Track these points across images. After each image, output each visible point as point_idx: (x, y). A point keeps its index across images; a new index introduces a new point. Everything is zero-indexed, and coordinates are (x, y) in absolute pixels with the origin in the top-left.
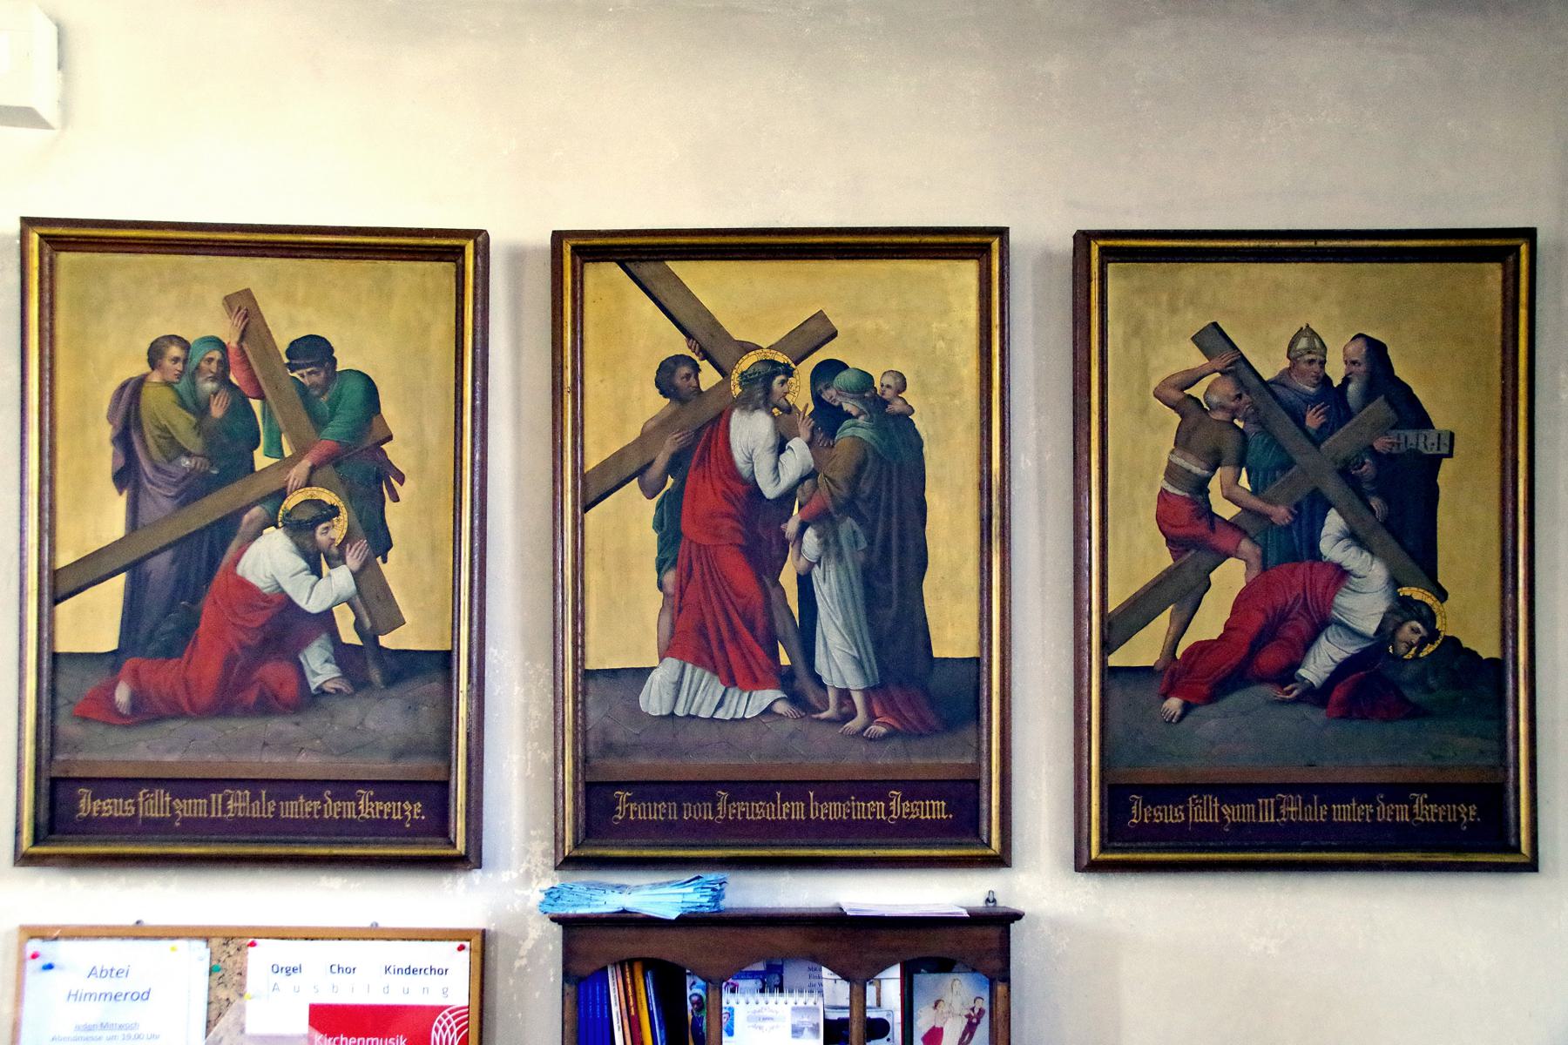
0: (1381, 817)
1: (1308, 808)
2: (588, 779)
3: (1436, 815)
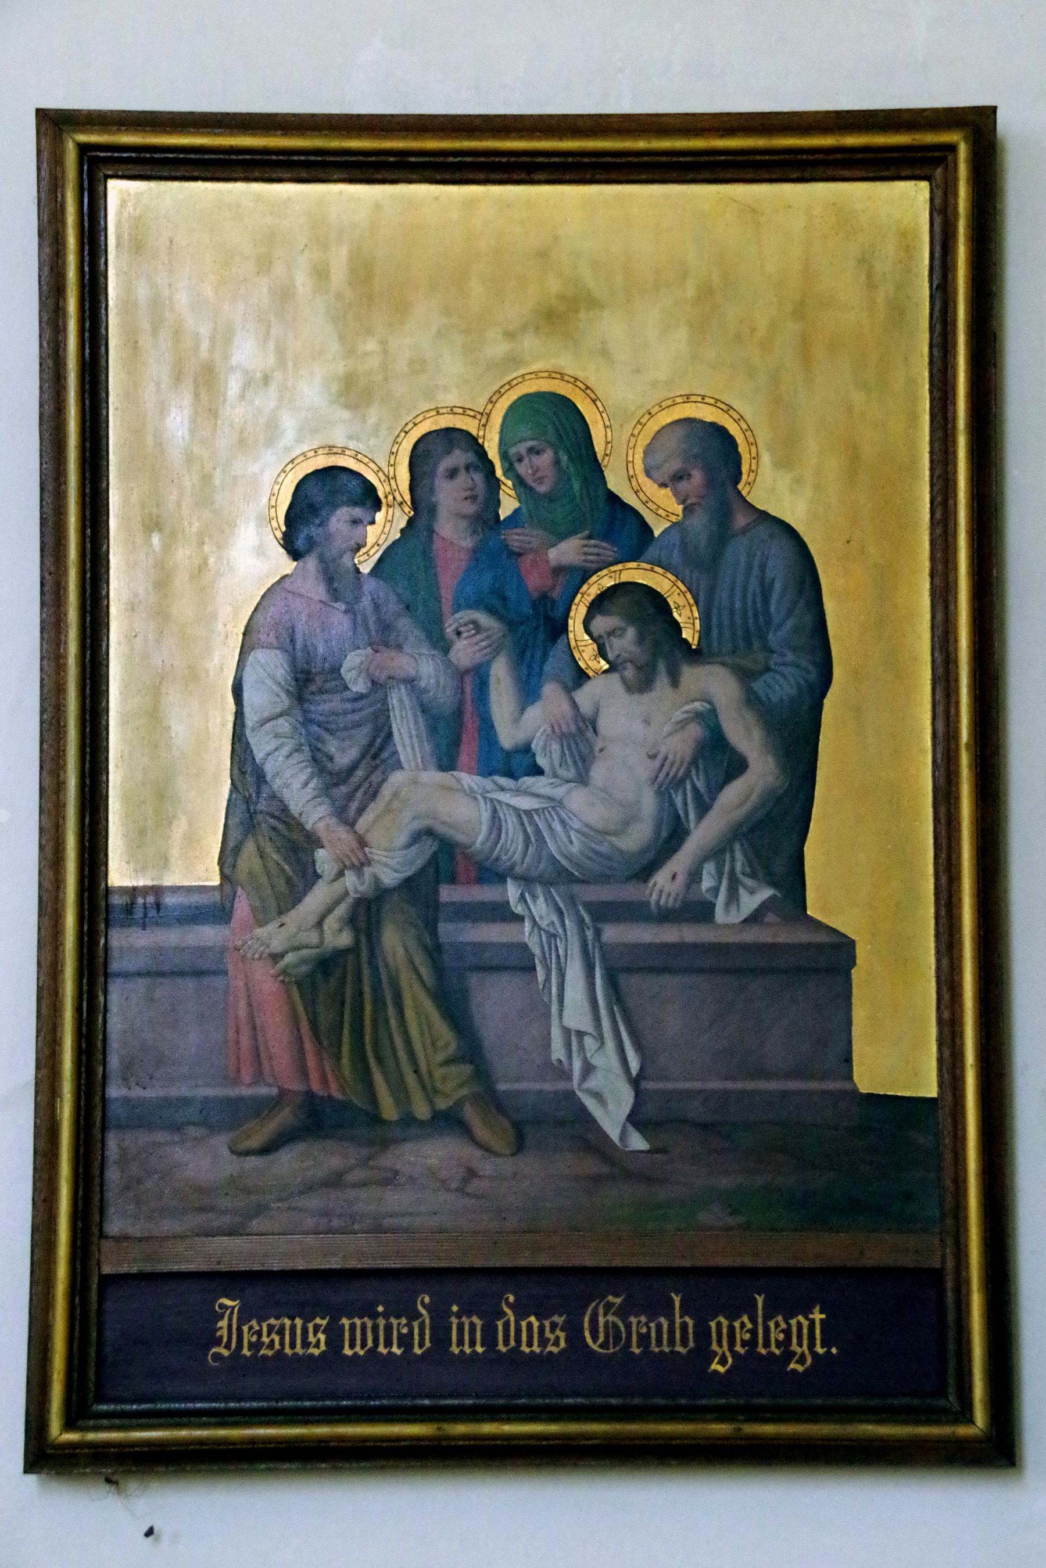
0: (506, 1342)
1: (719, 1325)
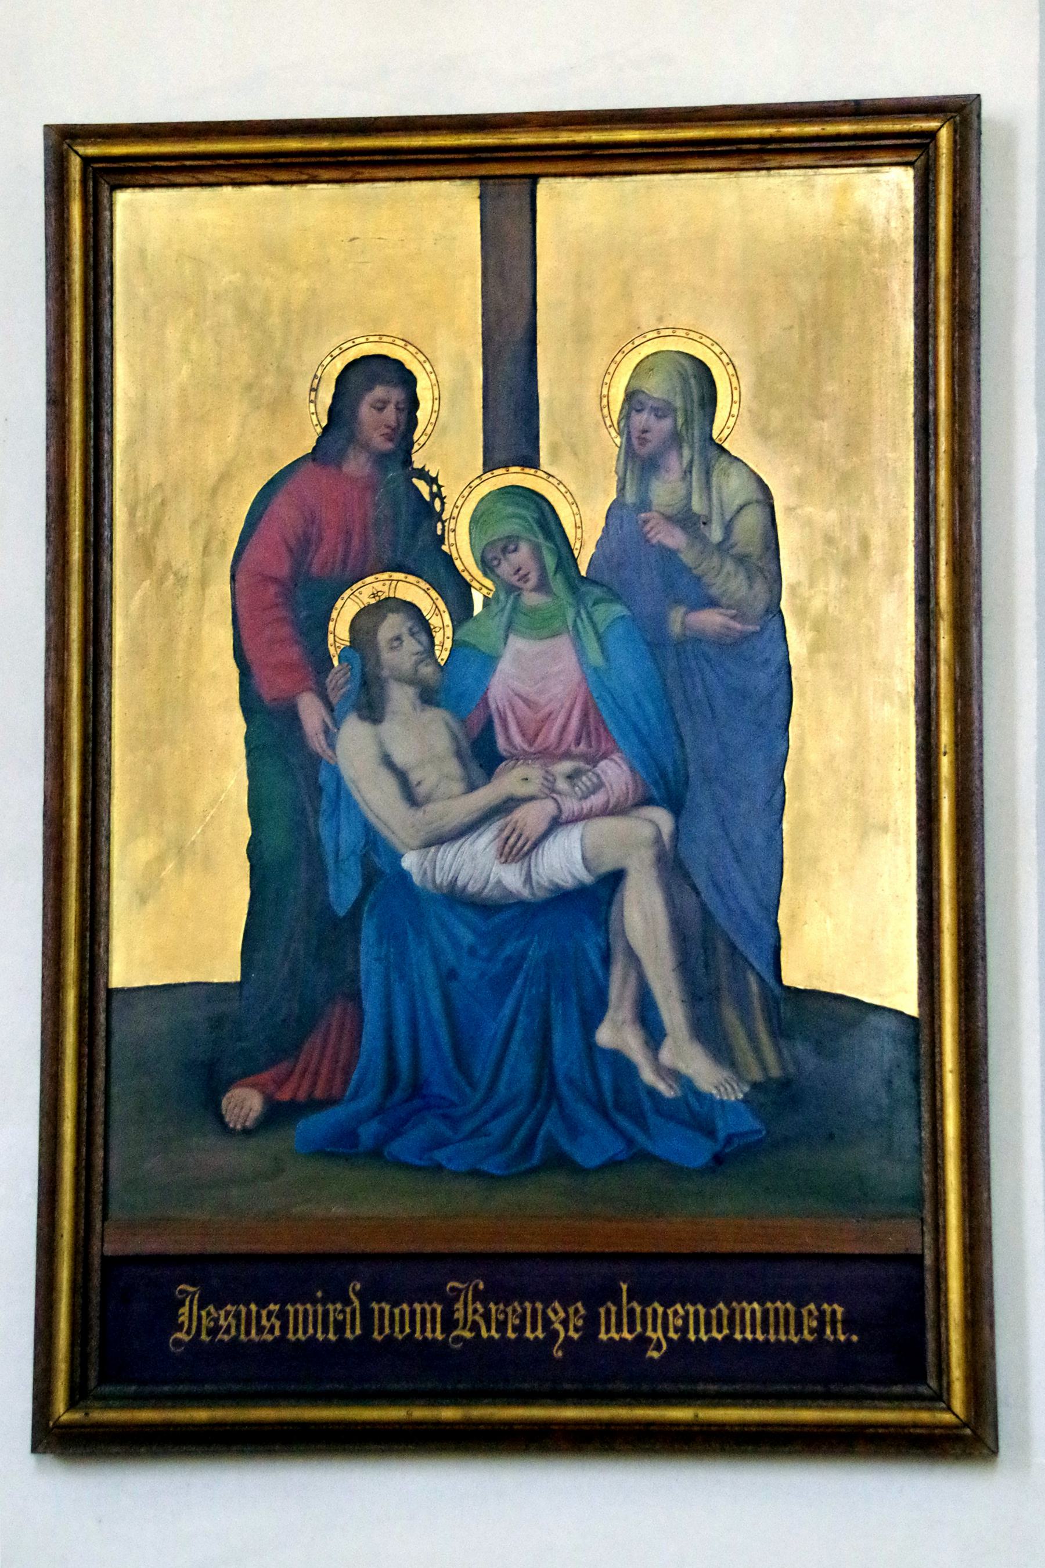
1: (655, 1311)
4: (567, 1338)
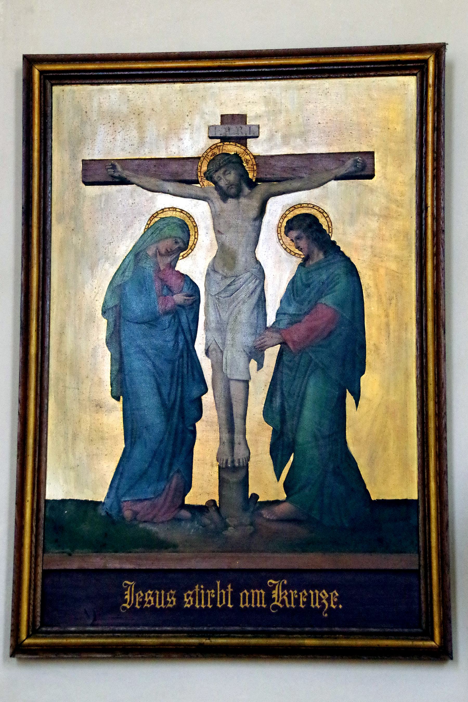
0: (221, 602)
1: (244, 594)
2: (44, 568)
3: (297, 601)
4: (330, 608)
